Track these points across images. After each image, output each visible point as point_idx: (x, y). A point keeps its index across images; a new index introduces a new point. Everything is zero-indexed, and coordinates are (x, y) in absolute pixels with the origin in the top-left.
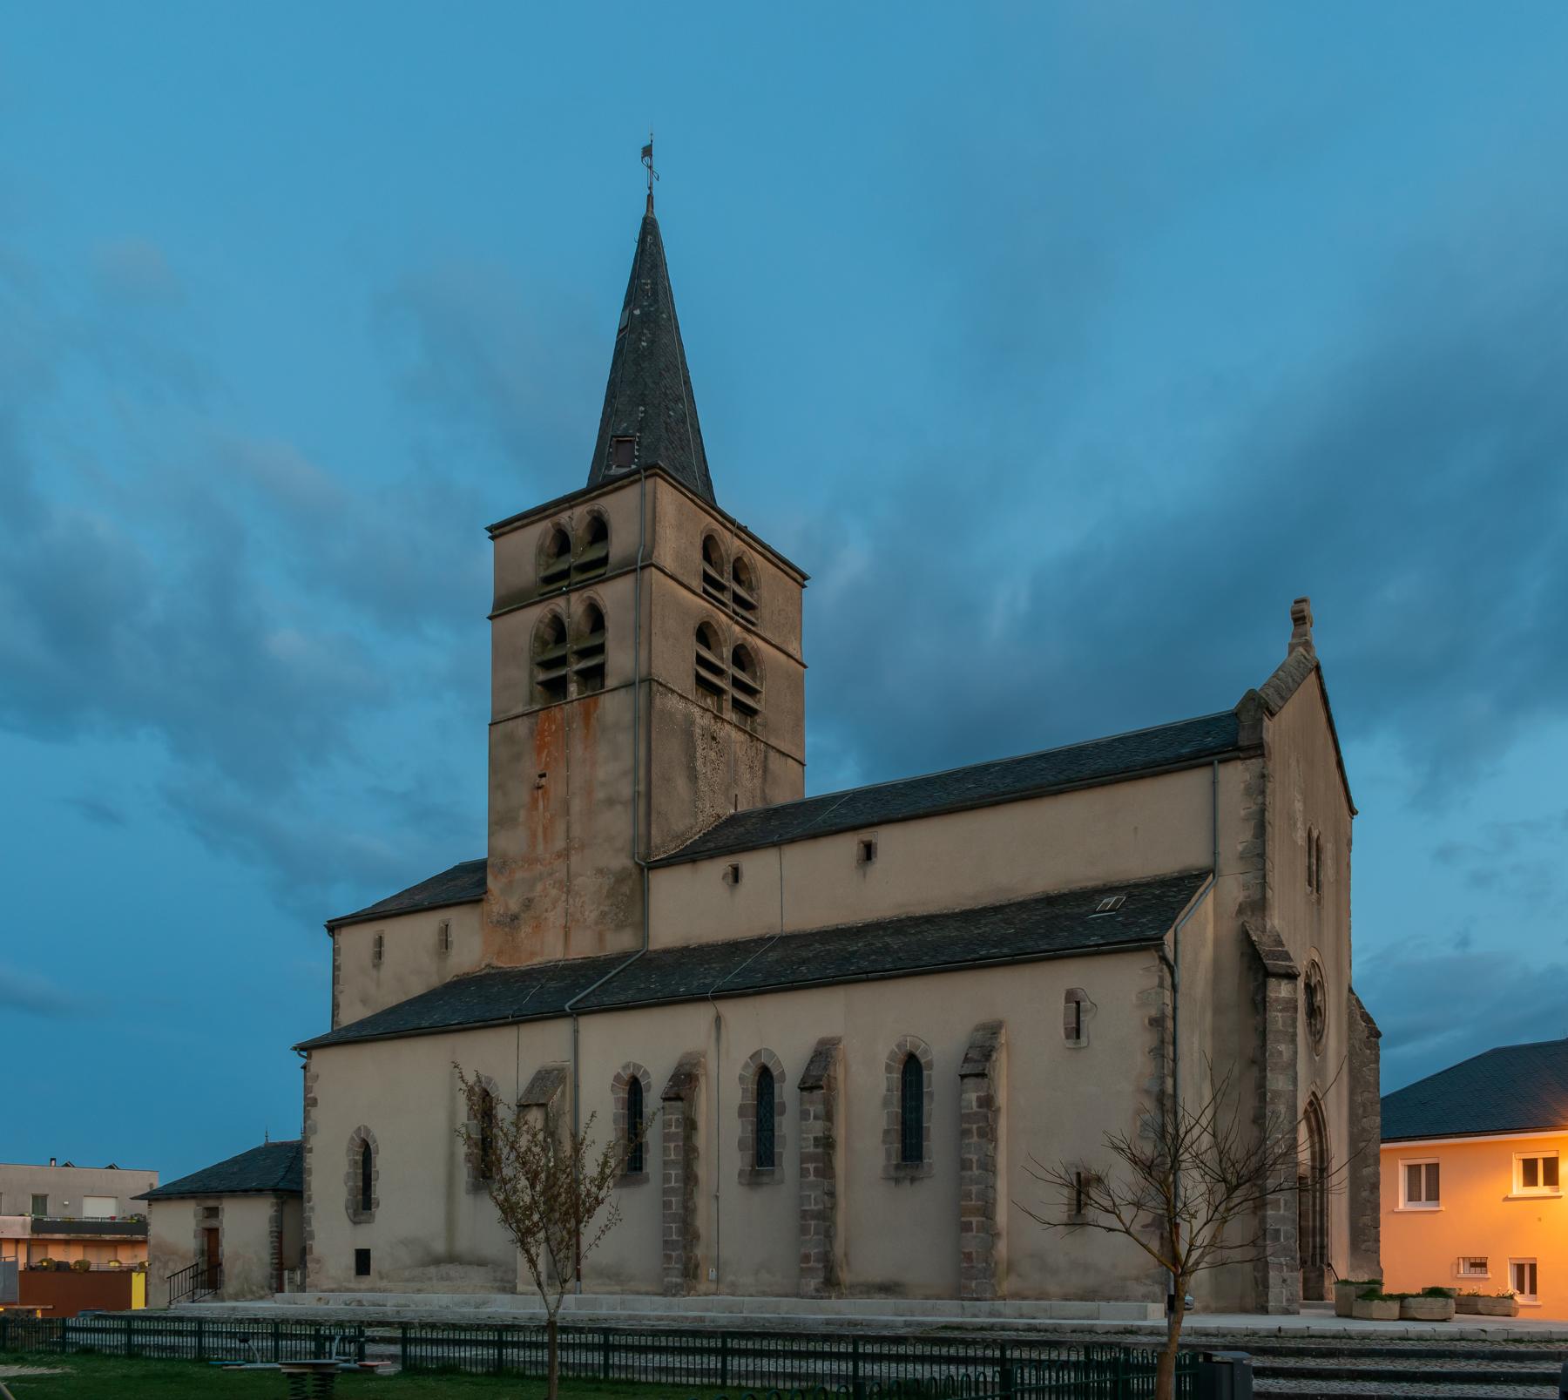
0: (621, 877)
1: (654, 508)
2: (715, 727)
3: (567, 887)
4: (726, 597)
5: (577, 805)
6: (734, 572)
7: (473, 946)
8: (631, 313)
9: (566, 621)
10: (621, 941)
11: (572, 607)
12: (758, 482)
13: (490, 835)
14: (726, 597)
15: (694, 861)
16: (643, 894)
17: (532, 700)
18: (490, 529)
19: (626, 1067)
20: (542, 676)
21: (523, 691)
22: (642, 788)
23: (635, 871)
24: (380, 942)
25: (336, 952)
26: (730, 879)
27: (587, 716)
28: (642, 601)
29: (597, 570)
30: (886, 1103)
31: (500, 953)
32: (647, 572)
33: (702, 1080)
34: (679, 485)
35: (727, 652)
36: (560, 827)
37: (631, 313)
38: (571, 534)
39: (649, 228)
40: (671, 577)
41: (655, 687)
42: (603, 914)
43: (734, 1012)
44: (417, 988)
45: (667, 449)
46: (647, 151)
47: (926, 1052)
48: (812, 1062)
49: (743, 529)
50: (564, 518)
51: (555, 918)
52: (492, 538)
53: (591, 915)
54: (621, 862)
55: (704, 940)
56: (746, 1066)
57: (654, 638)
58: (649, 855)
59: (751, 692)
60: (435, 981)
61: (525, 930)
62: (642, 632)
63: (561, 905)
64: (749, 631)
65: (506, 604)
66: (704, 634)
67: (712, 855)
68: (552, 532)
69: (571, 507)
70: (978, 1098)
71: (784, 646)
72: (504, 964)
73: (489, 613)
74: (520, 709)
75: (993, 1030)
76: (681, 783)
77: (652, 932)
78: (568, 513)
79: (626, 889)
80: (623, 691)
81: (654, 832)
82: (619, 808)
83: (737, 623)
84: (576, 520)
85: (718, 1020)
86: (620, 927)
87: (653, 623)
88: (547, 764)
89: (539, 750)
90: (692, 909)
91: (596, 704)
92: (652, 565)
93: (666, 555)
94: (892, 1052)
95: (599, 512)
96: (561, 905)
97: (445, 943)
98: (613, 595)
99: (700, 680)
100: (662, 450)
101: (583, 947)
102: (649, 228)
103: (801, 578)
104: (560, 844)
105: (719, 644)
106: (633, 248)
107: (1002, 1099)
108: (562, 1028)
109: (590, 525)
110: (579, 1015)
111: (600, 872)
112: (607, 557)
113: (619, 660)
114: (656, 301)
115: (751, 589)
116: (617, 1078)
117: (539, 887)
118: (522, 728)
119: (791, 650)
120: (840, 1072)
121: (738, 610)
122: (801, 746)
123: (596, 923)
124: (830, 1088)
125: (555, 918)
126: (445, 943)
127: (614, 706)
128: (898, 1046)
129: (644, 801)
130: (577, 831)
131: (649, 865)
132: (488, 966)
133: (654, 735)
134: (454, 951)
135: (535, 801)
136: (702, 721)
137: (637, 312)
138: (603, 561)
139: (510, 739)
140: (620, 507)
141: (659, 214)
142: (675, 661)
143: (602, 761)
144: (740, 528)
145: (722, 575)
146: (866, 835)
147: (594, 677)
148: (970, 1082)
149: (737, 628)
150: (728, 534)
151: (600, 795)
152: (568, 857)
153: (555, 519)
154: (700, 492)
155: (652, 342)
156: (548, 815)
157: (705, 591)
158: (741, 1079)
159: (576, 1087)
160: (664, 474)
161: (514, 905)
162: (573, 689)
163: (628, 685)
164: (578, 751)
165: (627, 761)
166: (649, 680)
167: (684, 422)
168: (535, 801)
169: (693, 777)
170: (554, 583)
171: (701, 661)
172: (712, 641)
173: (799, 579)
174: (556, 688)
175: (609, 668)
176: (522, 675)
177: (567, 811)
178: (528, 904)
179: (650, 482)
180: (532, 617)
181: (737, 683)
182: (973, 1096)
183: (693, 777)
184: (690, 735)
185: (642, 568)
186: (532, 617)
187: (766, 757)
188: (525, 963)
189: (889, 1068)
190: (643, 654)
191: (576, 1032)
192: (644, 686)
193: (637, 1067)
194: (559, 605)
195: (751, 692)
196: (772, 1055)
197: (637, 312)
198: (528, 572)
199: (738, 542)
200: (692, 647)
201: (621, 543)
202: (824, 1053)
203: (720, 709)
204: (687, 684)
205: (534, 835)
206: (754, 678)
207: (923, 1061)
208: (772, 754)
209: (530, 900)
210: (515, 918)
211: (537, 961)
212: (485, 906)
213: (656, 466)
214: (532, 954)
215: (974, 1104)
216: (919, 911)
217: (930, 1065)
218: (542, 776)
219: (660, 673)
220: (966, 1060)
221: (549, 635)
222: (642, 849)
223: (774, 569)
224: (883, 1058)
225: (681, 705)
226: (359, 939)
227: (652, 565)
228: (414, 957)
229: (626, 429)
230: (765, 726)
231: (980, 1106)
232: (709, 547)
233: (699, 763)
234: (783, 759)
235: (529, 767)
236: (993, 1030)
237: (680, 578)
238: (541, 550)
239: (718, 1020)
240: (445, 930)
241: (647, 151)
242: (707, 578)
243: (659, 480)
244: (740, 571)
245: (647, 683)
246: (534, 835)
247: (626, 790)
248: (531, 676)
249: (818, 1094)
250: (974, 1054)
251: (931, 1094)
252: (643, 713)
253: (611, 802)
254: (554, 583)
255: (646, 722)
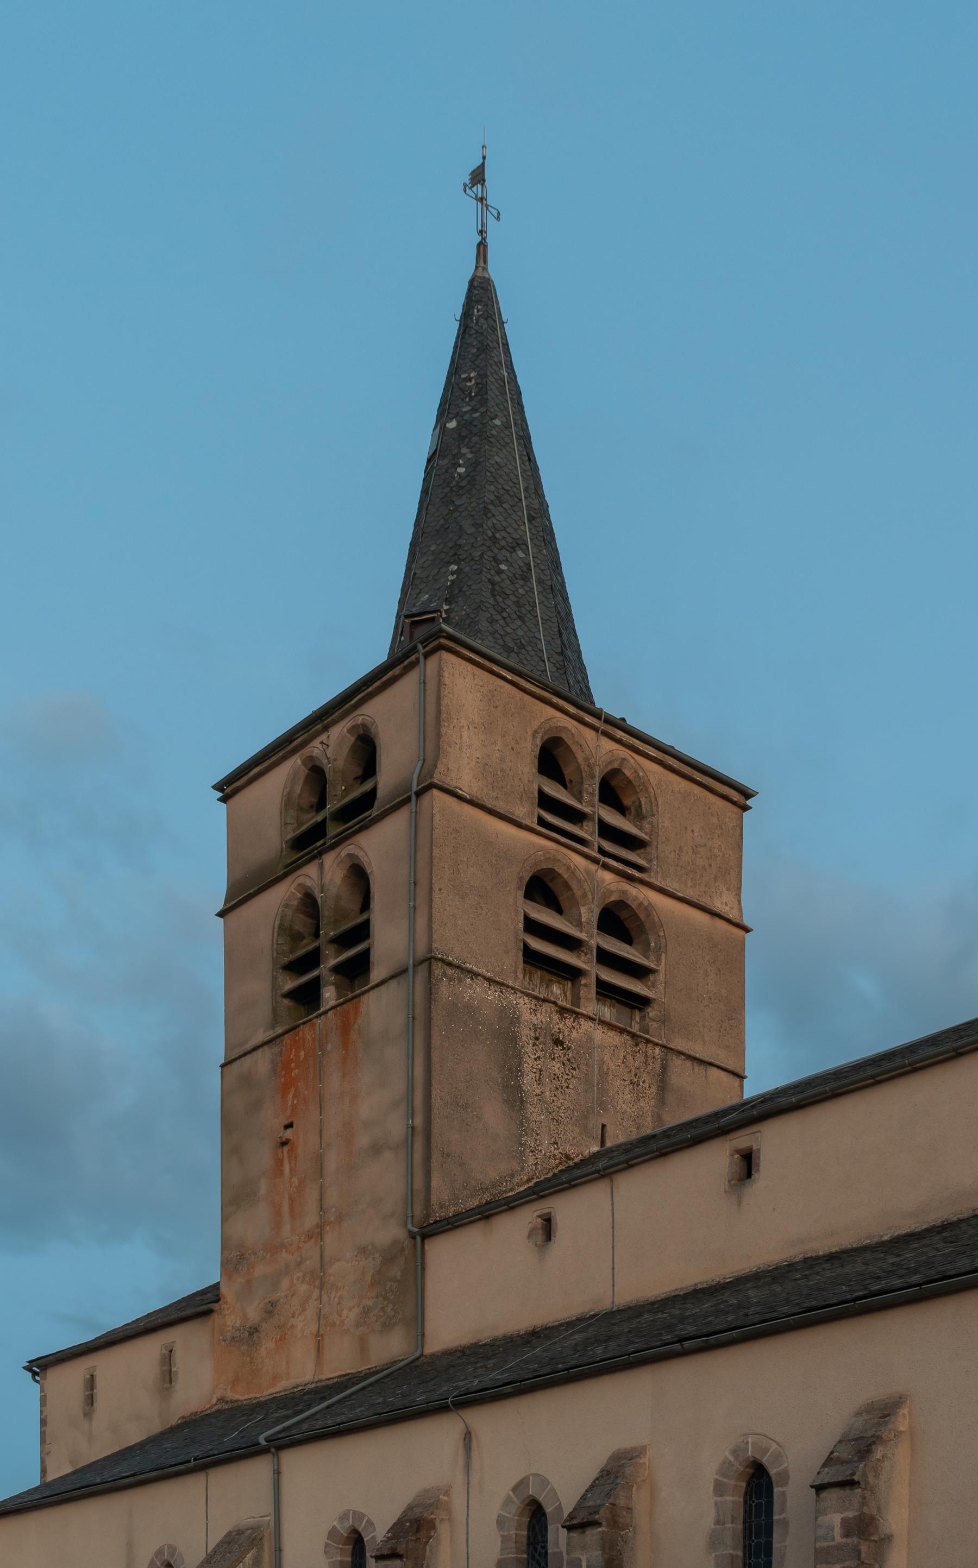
0: (389, 1257)
1: (439, 699)
2: (564, 1026)
3: (319, 1279)
4: (587, 831)
5: (332, 1161)
6: (606, 798)
7: (202, 1377)
8: (444, 428)
9: (319, 896)
10: (390, 1347)
11: (326, 875)
12: (646, 656)
13: (225, 1219)
14: (587, 831)
15: (487, 1217)
16: (417, 1271)
17: (275, 1021)
18: (219, 787)
19: (343, 1517)
20: (290, 984)
21: (263, 1010)
22: (419, 1121)
23: (408, 1243)
24: (91, 1383)
25: (43, 1401)
26: (540, 1237)
27: (345, 1029)
28: (417, 845)
29: (360, 811)
30: (714, 1541)
31: (235, 1382)
32: (426, 798)
33: (443, 1530)
34: (484, 661)
35: (589, 913)
36: (311, 1196)
37: (444, 428)
38: (327, 767)
39: (480, 294)
40: (471, 802)
41: (438, 969)
42: (366, 1311)
43: (489, 1422)
44: (134, 1436)
45: (492, 621)
46: (478, 176)
47: (778, 1457)
48: (592, 1486)
49: (620, 724)
50: (315, 748)
51: (304, 1324)
52: (224, 799)
53: (351, 1315)
54: (390, 1233)
55: (500, 1332)
56: (507, 1502)
57: (436, 896)
58: (427, 1216)
59: (639, 972)
60: (156, 1427)
61: (267, 1345)
62: (419, 889)
63: (312, 1306)
64: (630, 879)
65: (240, 895)
66: (542, 887)
67: (511, 1204)
68: (304, 771)
69: (326, 729)
70: (844, 1521)
71: (705, 901)
72: (241, 1395)
73: (220, 906)
74: (261, 1036)
75: (884, 1412)
76: (492, 1113)
77: (430, 1327)
78: (323, 737)
79: (395, 1271)
80: (393, 983)
81: (436, 1182)
82: (388, 1155)
83: (606, 867)
84: (334, 746)
85: (468, 1437)
86: (387, 1326)
87: (453, 879)
88: (294, 1108)
89: (284, 1090)
90: (485, 1288)
91: (357, 1009)
92: (432, 786)
93: (462, 769)
94: (725, 1462)
95: (364, 726)
96: (312, 1306)
97: (168, 1376)
98: (379, 845)
99: (531, 958)
100: (484, 625)
101: (341, 1360)
102: (480, 294)
103: (739, 796)
104: (311, 1220)
105: (575, 903)
106: (452, 329)
107: (896, 1518)
108: (259, 1469)
109: (354, 750)
110: (280, 1448)
111: (363, 1251)
112: (374, 791)
113: (389, 942)
114: (484, 402)
115: (639, 817)
116: (333, 1533)
117: (285, 1283)
118: (261, 1063)
119: (718, 906)
120: (640, 1499)
121: (608, 846)
122: (739, 1049)
123: (358, 1325)
124: (614, 1523)
125: (304, 1324)
126: (168, 1376)
127: (381, 1008)
128: (734, 1452)
129: (422, 1140)
130: (333, 1197)
131: (430, 1229)
132: (221, 1400)
133: (436, 1041)
134: (179, 1384)
135: (279, 1163)
136: (531, 1016)
137: (452, 425)
138: (371, 796)
139: (247, 1081)
140: (389, 716)
141: (495, 271)
142: (483, 928)
143: (366, 1094)
144: (609, 721)
145: (580, 799)
146: (742, 1140)
147: (356, 971)
148: (831, 1496)
149: (608, 877)
150: (589, 734)
151: (363, 1140)
152: (321, 1236)
153: (306, 752)
154: (563, 680)
155: (474, 466)
156: (295, 1181)
157: (542, 822)
158: (500, 1522)
159: (279, 1550)
160: (457, 647)
161: (253, 1313)
162: (329, 995)
163: (399, 974)
164: (334, 1081)
165: (398, 1086)
166: (429, 960)
167: (526, 578)
168: (279, 1163)
169: (515, 1099)
170: (307, 844)
171: (532, 926)
172: (563, 899)
173: (736, 796)
174: (307, 997)
175: (375, 956)
176: (263, 986)
177: (320, 1170)
178: (271, 1309)
179: (433, 662)
180: (280, 897)
181: (605, 958)
182: (835, 1519)
183: (515, 1099)
184: (513, 1039)
185: (419, 794)
186: (280, 897)
187: (664, 1068)
188: (266, 1392)
189: (719, 1489)
190: (421, 922)
191: (278, 1473)
192: (423, 969)
193: (359, 1516)
194: (309, 875)
195: (639, 972)
196: (544, 1482)
197: (452, 425)
198: (272, 838)
199: (608, 745)
200: (516, 907)
201: (393, 768)
202: (616, 1474)
203: (576, 1001)
204: (509, 963)
205: (278, 1213)
206: (645, 952)
207: (772, 1472)
208: (677, 1063)
209: (273, 1304)
210: (254, 1330)
211: (282, 1386)
212: (216, 1319)
213: (440, 633)
214: (275, 1378)
215: (837, 1532)
216: (823, 1247)
217: (785, 1477)
218: (289, 1126)
219: (450, 944)
220: (830, 1461)
221: (301, 924)
222: (418, 1210)
223: (684, 784)
224: (709, 1473)
225: (492, 995)
226: (69, 1379)
227: (432, 786)
228: (131, 1401)
229: (430, 601)
230: (663, 1021)
231: (847, 1535)
232: (552, 758)
233: (528, 1081)
234: (699, 1069)
235: (271, 1118)
236: (884, 1412)
237: (489, 804)
238: (288, 801)
239: (468, 1437)
240: (168, 1357)
241: (478, 176)
242: (545, 801)
243: (445, 655)
244: (612, 790)
245: (427, 964)
246: (278, 1213)
247: (396, 1127)
248: (274, 986)
249: (593, 1534)
250: (843, 1453)
251: (785, 1523)
252: (419, 1011)
253: (376, 1149)
254: (307, 844)
255: (422, 1022)
